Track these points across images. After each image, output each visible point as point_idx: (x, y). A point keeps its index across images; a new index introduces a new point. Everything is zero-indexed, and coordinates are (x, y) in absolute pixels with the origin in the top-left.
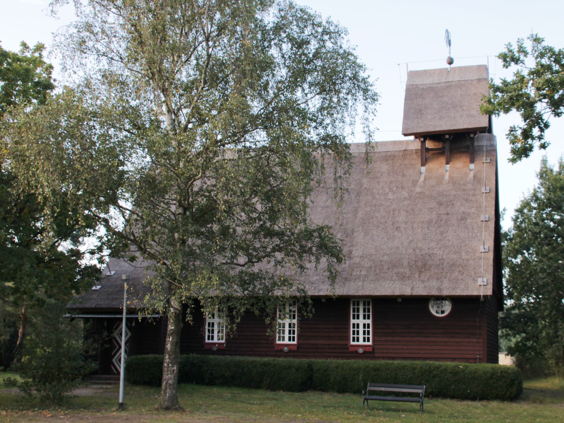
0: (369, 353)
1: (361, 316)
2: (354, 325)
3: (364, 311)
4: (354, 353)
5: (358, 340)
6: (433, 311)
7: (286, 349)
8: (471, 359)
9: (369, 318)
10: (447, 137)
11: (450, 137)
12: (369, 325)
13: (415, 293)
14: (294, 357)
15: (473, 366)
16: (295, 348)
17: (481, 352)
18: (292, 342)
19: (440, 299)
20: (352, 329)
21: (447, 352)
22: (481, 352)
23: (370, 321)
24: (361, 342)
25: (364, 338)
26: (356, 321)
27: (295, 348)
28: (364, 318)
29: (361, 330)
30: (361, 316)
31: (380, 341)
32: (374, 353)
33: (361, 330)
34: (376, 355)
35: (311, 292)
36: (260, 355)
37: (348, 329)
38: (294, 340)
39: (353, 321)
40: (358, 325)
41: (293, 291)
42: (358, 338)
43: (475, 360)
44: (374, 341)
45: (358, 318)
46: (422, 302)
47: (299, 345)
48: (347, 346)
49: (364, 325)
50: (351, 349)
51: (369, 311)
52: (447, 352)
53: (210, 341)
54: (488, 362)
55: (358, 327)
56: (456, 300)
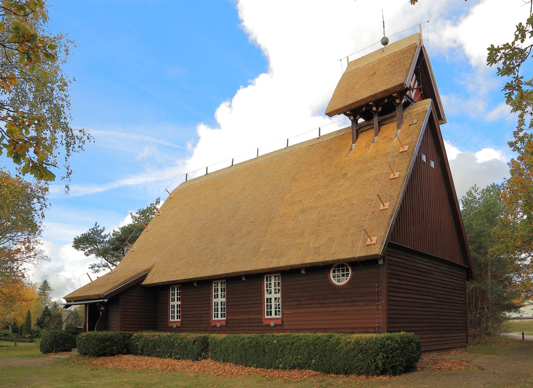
0: (279, 327)
4: (268, 328)
5: (271, 315)
9: (267, 299)
24: (273, 316)
34: (285, 327)
37: (262, 303)
48: (260, 320)
50: (265, 323)
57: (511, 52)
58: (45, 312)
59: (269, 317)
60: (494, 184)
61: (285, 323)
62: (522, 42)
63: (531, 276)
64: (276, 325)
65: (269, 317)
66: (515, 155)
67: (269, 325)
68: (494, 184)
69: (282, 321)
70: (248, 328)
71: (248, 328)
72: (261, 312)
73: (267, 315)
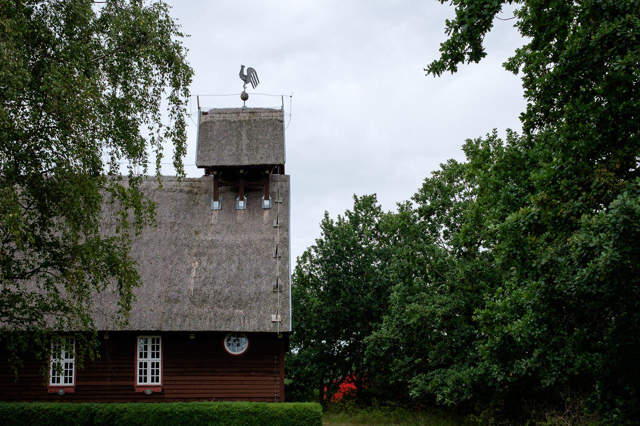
0: (157, 396)
1: (63, 356)
2: (141, 364)
3: (153, 349)
4: (142, 396)
5: (145, 381)
6: (229, 350)
7: (61, 391)
8: (268, 397)
9: (158, 357)
10: (242, 171)
11: (245, 172)
12: (158, 364)
13: (262, 329)
14: (71, 400)
15: (274, 405)
16: (73, 391)
17: (278, 391)
18: (68, 384)
19: (238, 335)
20: (138, 369)
21: (243, 391)
22: (278, 391)
23: (159, 360)
24: (149, 382)
25: (153, 378)
26: (143, 360)
27: (73, 391)
28: (153, 357)
29: (149, 370)
30: (63, 356)
31: (171, 380)
32: (164, 394)
33: (149, 370)
34: (166, 396)
35: (99, 325)
36: (30, 400)
37: (134, 368)
38: (71, 382)
39: (139, 360)
40: (146, 364)
41: (77, 325)
42: (145, 378)
43: (272, 399)
44: (163, 381)
45: (146, 357)
46: (215, 339)
47: (77, 387)
48: (133, 387)
49: (153, 364)
50: (137, 390)
51: (158, 349)
52: (243, 391)
53: (56, 384)
54: (285, 401)
55: (146, 366)
56: (252, 336)
57: (554, 330)
58: (340, 256)
59: (143, 384)
60: (441, 44)
61: (166, 391)
62: (181, 74)
63: (98, 8)
64: (153, 393)
65: (143, 384)
66: (397, 212)
67: (143, 393)
68: (441, 44)
69: (162, 389)
70: (110, 397)
71: (110, 397)
72: (133, 378)
73: (141, 381)
